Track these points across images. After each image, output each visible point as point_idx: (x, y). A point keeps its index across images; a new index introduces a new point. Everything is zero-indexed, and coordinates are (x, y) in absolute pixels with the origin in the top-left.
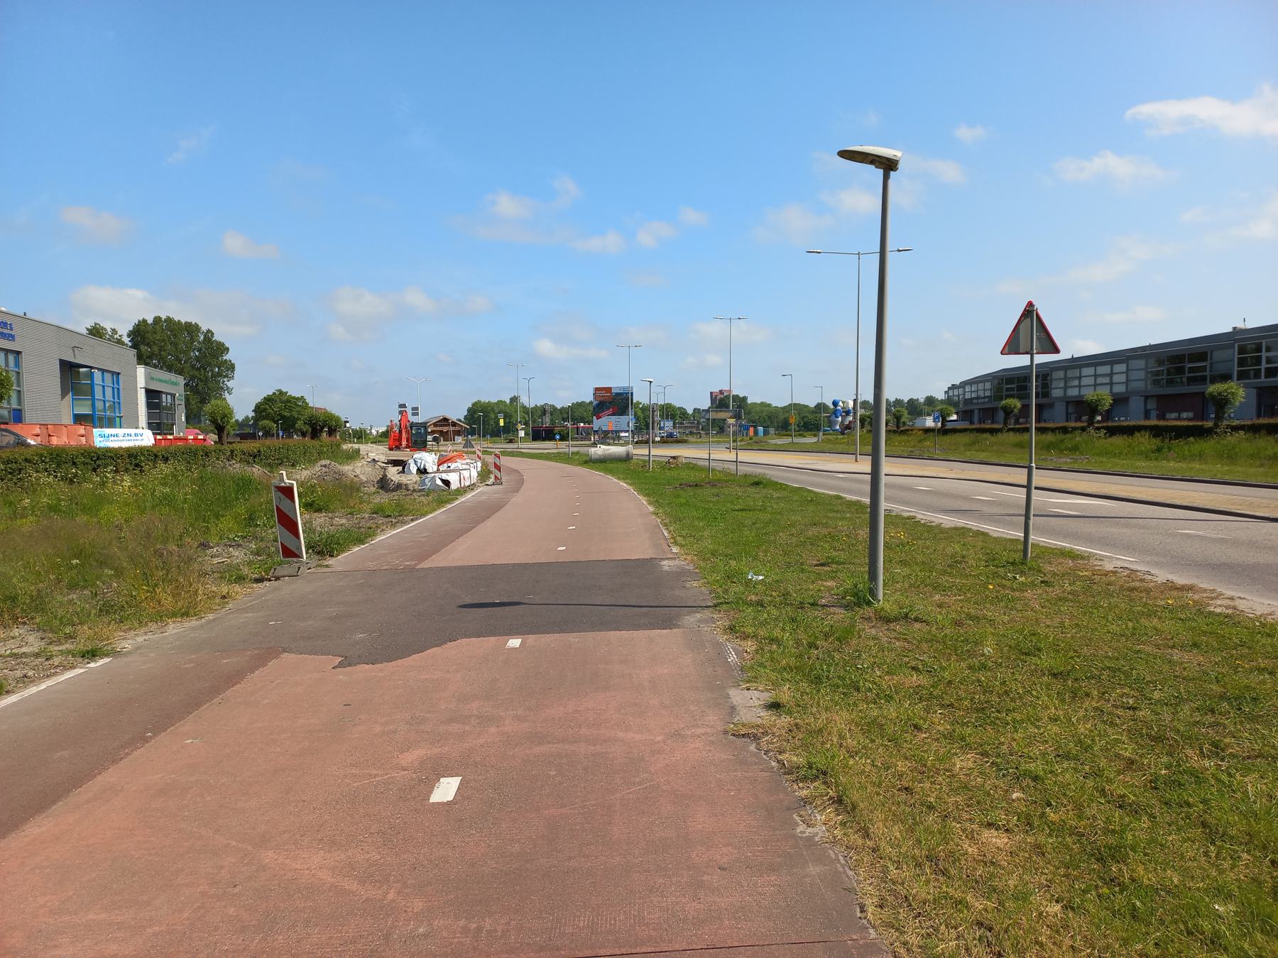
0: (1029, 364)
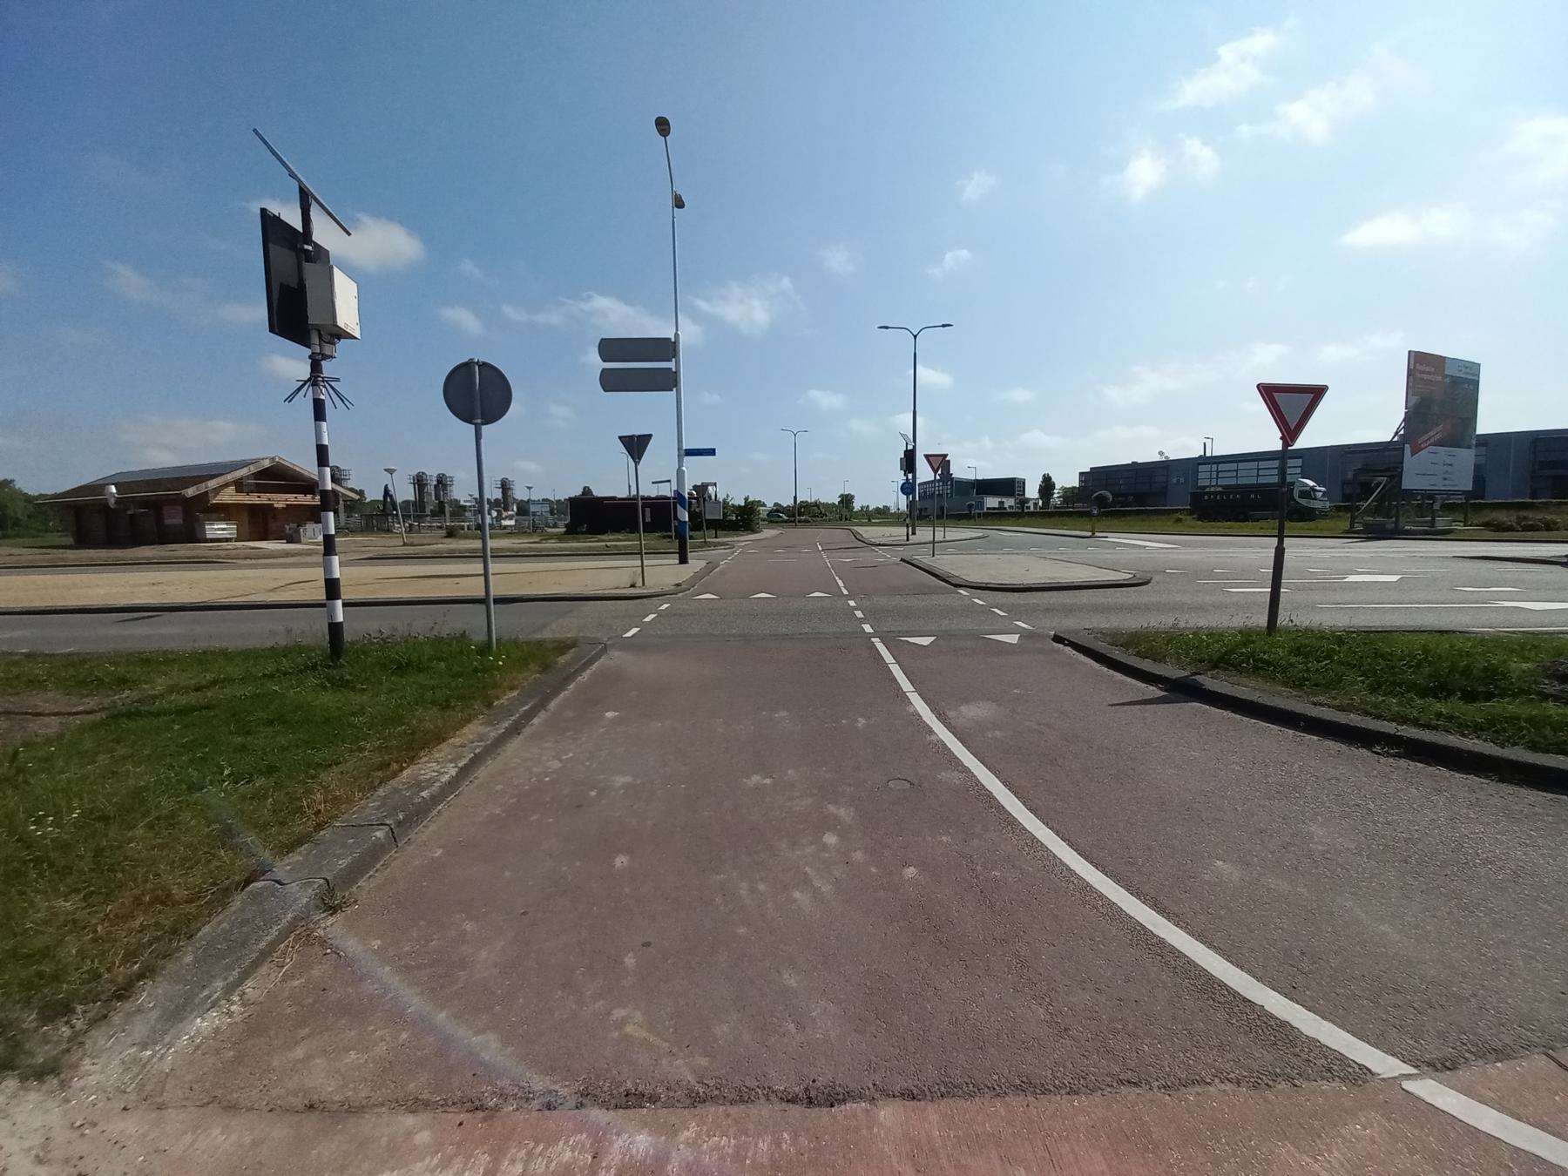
0: (208, 536)
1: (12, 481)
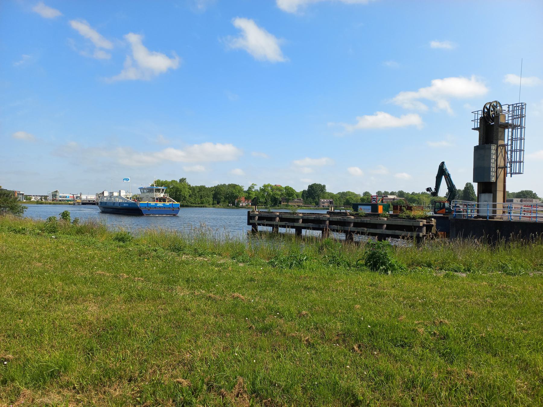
1: (185, 179)
